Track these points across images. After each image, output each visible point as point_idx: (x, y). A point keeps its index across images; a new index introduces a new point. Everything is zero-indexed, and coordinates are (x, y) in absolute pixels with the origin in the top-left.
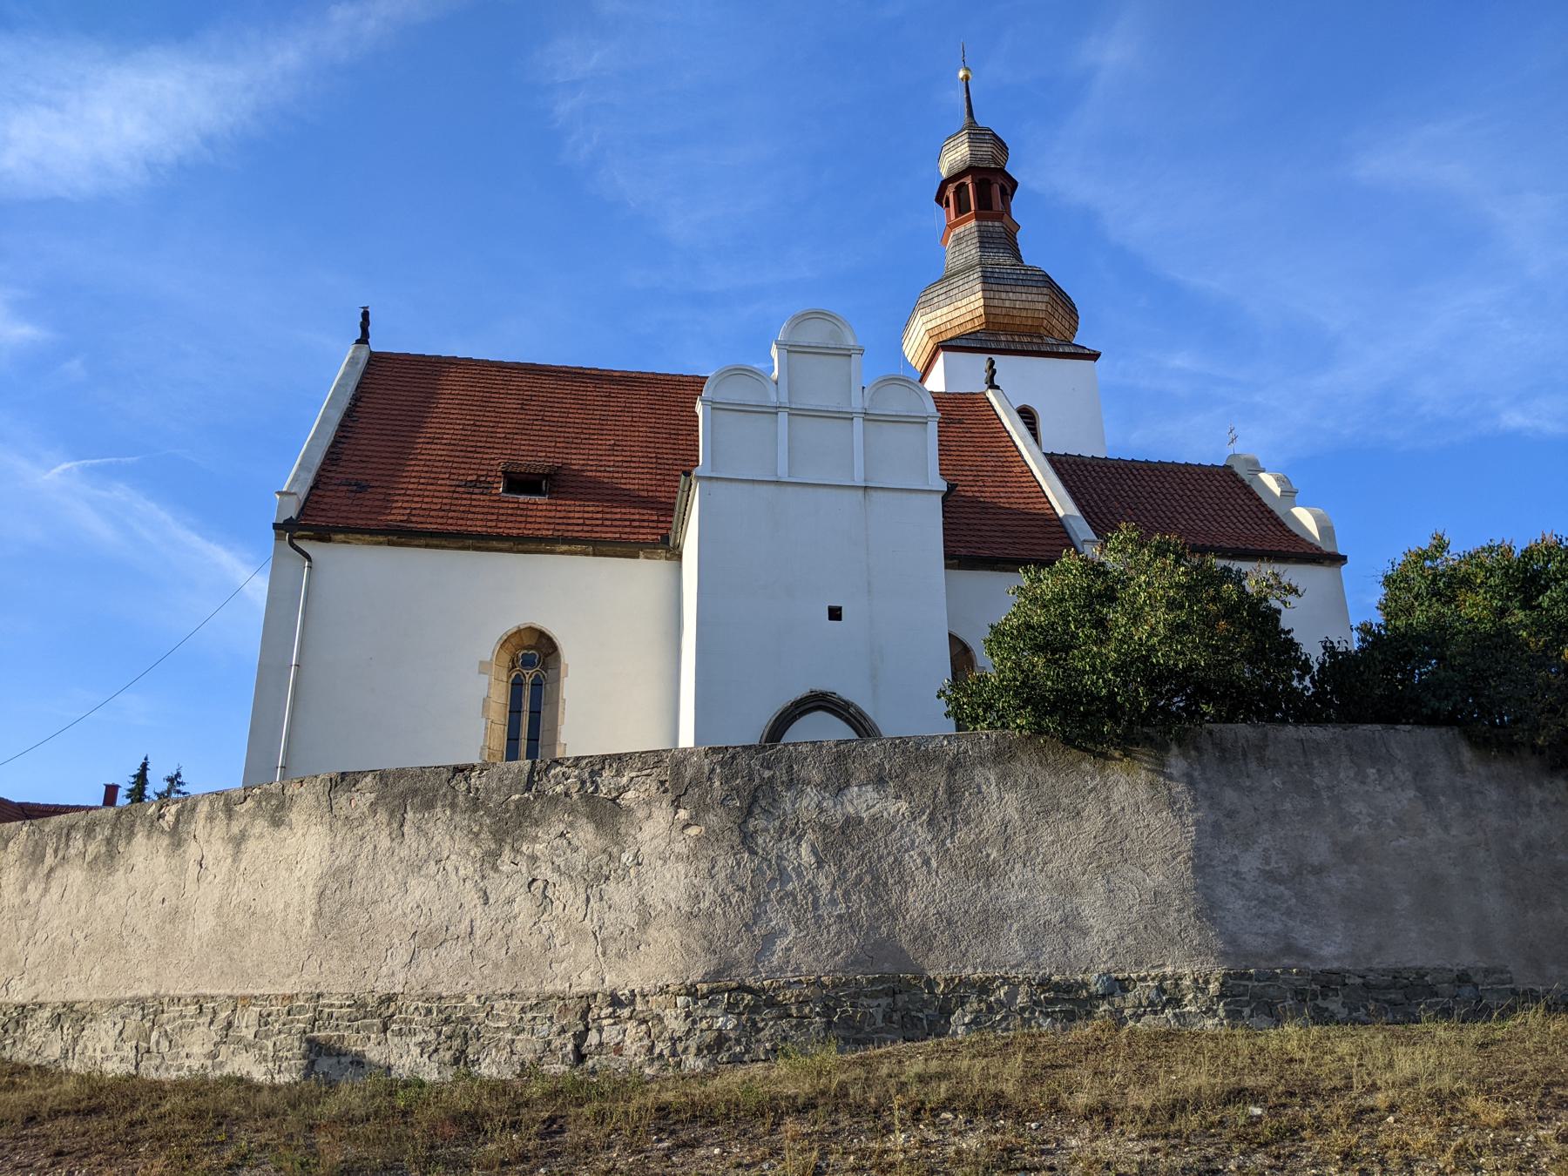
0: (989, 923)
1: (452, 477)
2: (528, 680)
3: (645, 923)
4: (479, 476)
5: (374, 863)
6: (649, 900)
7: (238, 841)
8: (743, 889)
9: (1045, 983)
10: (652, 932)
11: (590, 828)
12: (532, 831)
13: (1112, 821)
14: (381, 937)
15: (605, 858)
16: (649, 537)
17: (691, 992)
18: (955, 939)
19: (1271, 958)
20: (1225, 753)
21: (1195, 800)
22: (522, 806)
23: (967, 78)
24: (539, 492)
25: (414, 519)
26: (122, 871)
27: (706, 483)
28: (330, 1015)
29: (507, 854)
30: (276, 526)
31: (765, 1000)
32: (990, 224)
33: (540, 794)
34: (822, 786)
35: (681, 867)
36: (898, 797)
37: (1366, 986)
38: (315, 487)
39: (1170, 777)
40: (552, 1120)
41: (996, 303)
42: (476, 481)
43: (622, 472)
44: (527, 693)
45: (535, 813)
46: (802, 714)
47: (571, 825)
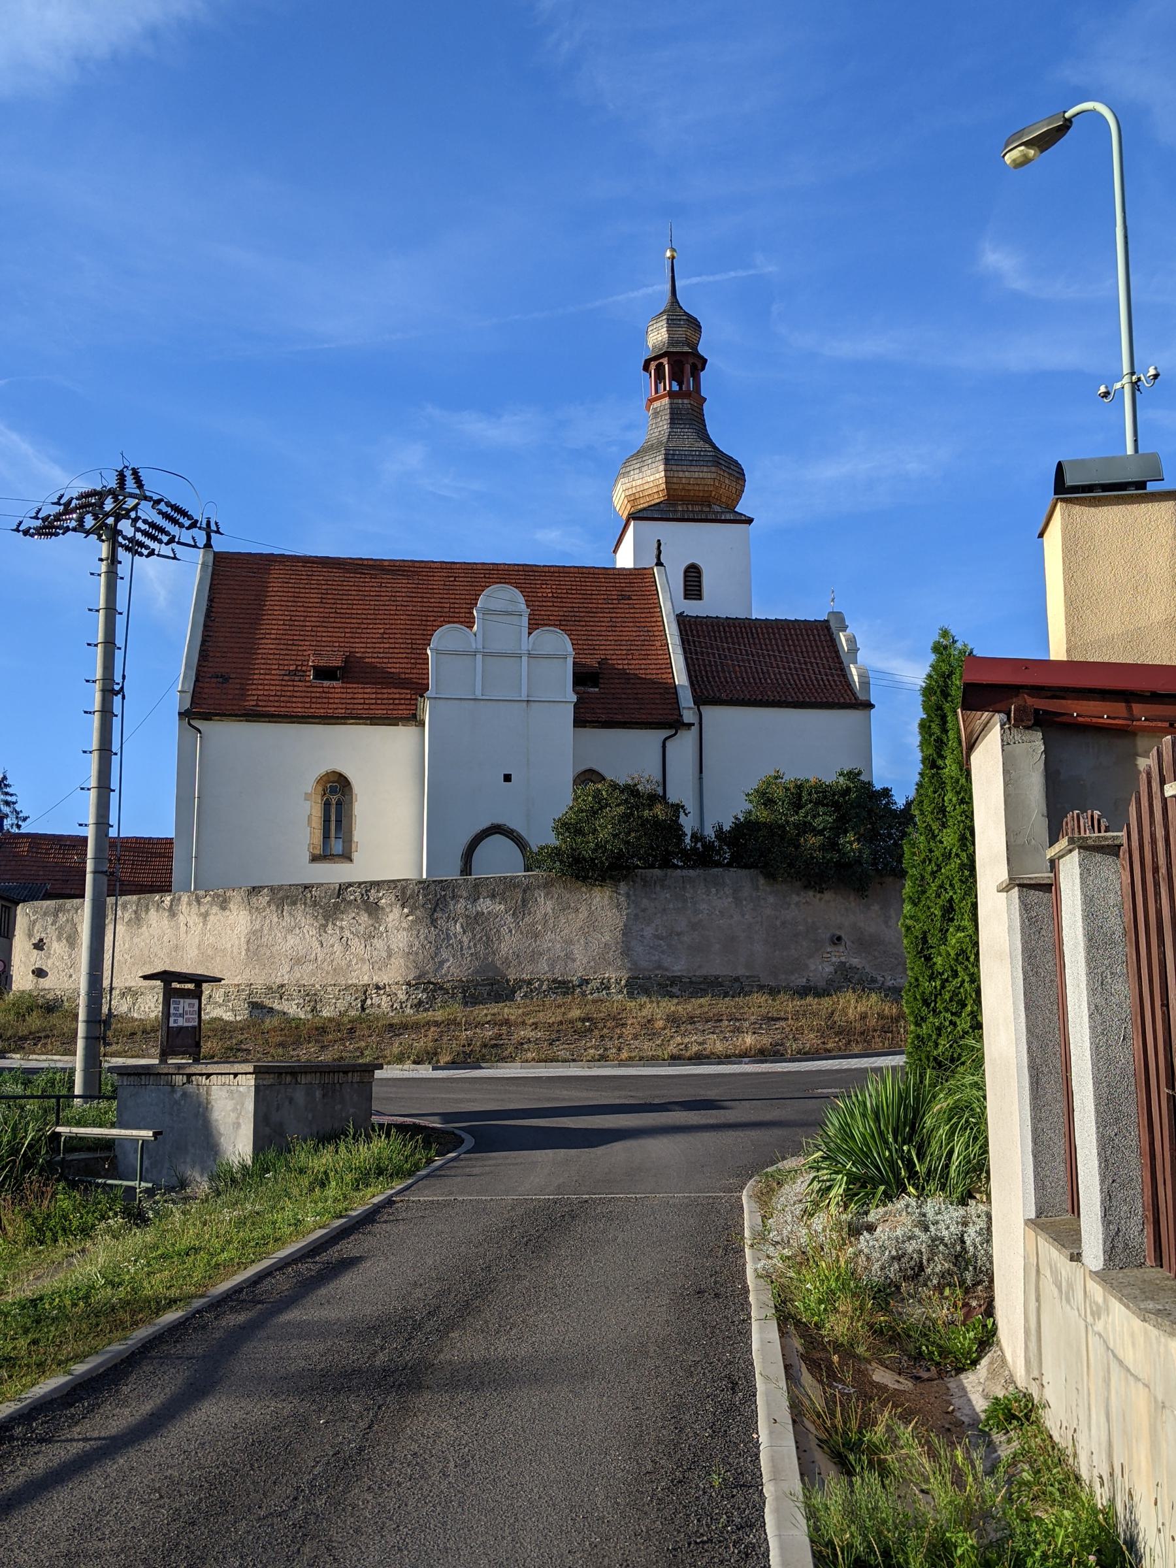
0: (534, 957)
1: (281, 667)
2: (334, 802)
3: (389, 956)
4: (297, 666)
5: (271, 929)
6: (391, 947)
7: (205, 916)
8: (431, 943)
9: (555, 981)
10: (393, 959)
11: (366, 915)
12: (341, 916)
13: (591, 913)
14: (276, 960)
15: (373, 928)
16: (405, 712)
17: (408, 984)
18: (520, 963)
19: (650, 971)
20: (646, 883)
21: (628, 904)
22: (336, 905)
23: (673, 258)
24: (334, 678)
25: (260, 703)
26: (145, 927)
27: (432, 700)
28: (257, 993)
29: (330, 926)
30: (180, 714)
31: (439, 987)
32: (680, 401)
33: (344, 900)
34: (467, 899)
35: (405, 933)
36: (500, 903)
37: (691, 982)
38: (197, 680)
39: (619, 894)
40: (352, 1029)
41: (675, 480)
42: (296, 670)
43: (389, 658)
44: (333, 811)
45: (342, 908)
46: (487, 836)
47: (358, 913)
